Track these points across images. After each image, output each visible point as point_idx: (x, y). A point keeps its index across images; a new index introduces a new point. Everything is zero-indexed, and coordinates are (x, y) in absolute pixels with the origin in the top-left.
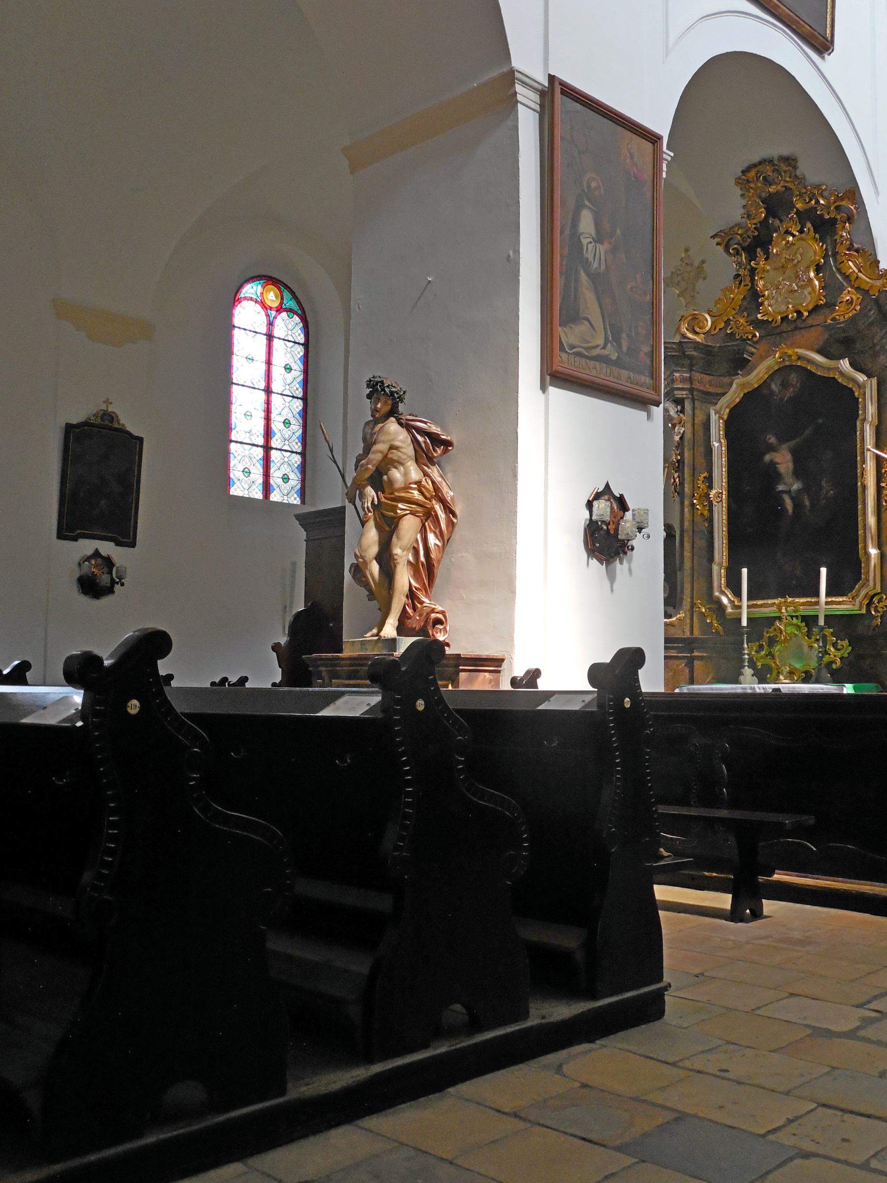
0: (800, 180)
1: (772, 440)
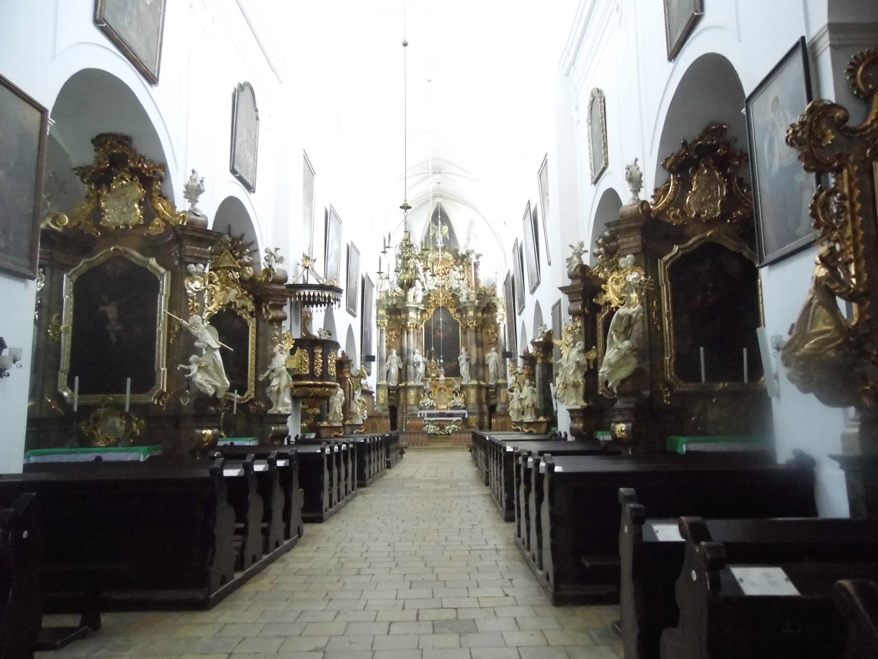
0: (134, 152)
1: (106, 299)
